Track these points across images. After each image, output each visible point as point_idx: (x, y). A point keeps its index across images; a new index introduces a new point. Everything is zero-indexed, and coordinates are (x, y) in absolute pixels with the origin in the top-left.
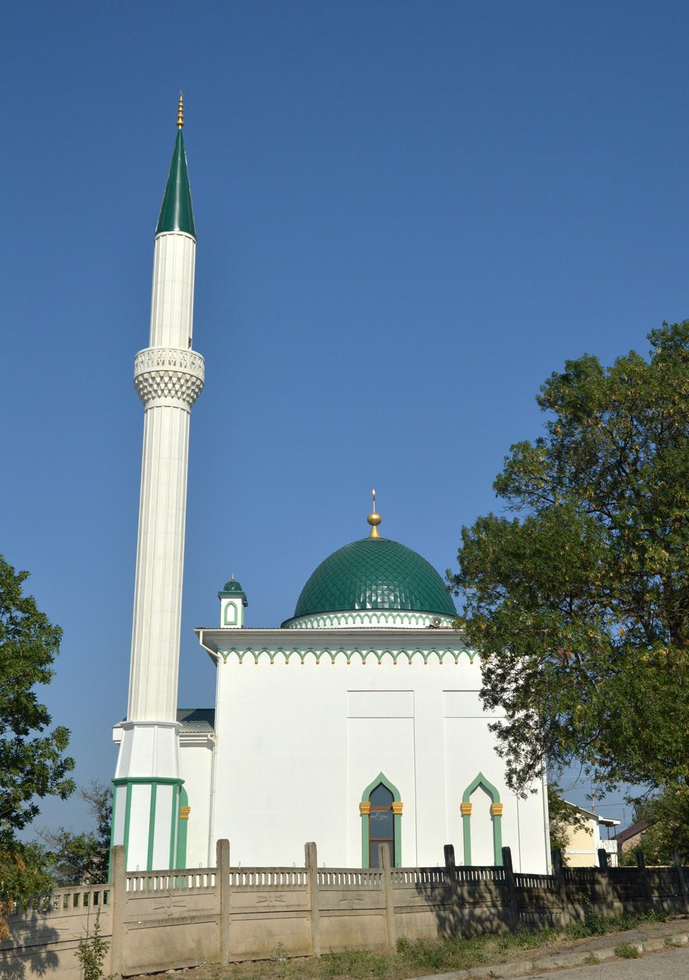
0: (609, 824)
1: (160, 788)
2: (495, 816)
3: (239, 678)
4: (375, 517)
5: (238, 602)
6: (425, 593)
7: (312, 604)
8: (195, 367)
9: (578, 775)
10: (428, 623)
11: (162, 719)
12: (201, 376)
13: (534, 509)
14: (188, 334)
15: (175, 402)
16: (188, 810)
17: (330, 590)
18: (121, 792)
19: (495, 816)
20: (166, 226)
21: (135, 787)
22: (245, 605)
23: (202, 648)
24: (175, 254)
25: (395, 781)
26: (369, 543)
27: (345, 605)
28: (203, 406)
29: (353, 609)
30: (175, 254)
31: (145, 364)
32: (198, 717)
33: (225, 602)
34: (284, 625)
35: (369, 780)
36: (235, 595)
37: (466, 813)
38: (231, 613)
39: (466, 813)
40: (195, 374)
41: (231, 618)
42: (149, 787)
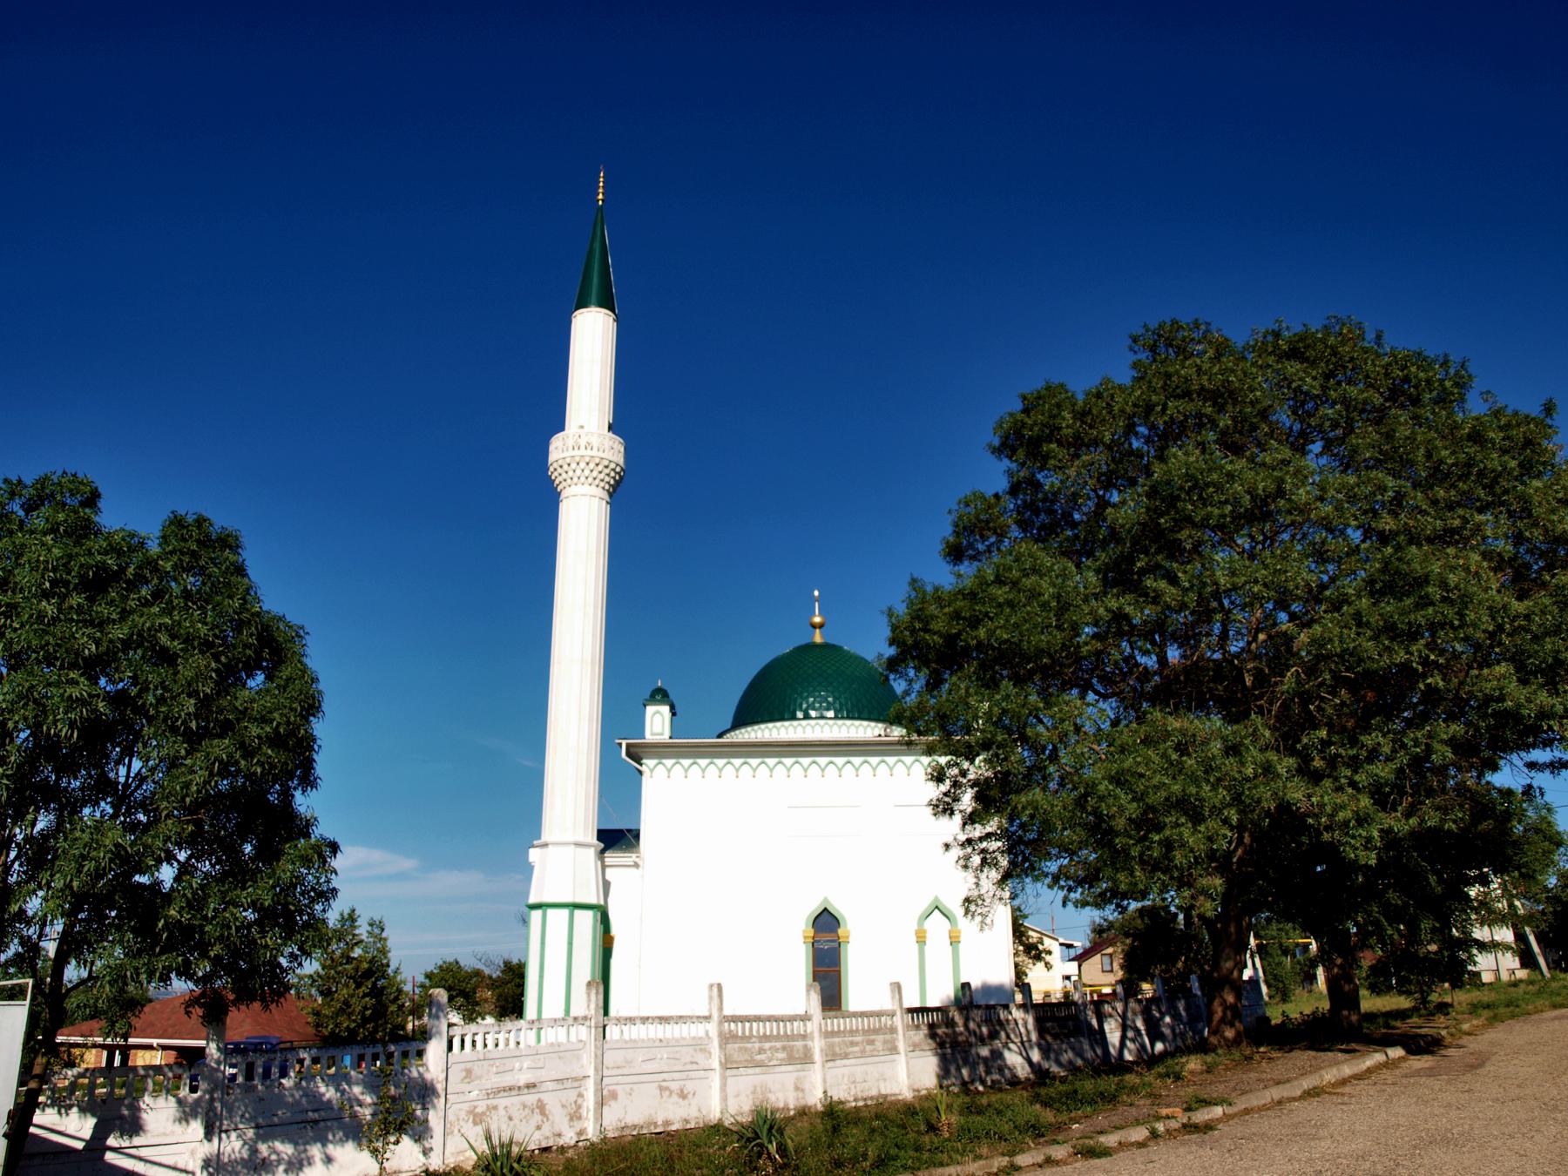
0: (1069, 946)
1: (577, 913)
2: (954, 941)
3: (666, 790)
4: (817, 620)
5: (665, 709)
6: (863, 696)
7: (744, 717)
8: (612, 450)
9: (1043, 899)
10: (877, 732)
11: (581, 839)
12: (621, 462)
13: (1487, 406)
14: (607, 416)
15: (587, 489)
16: (612, 939)
17: (768, 697)
18: (536, 915)
19: (954, 941)
20: (582, 303)
21: (550, 912)
22: (674, 714)
23: (623, 758)
24: (592, 336)
25: (839, 907)
26: (812, 646)
27: (783, 712)
28: (620, 492)
29: (794, 718)
30: (592, 336)
31: (559, 450)
32: (616, 839)
33: (650, 710)
34: (720, 736)
35: (813, 908)
36: (661, 702)
37: (921, 939)
38: (657, 722)
39: (921, 939)
40: (614, 459)
41: (657, 729)
42: (565, 912)
